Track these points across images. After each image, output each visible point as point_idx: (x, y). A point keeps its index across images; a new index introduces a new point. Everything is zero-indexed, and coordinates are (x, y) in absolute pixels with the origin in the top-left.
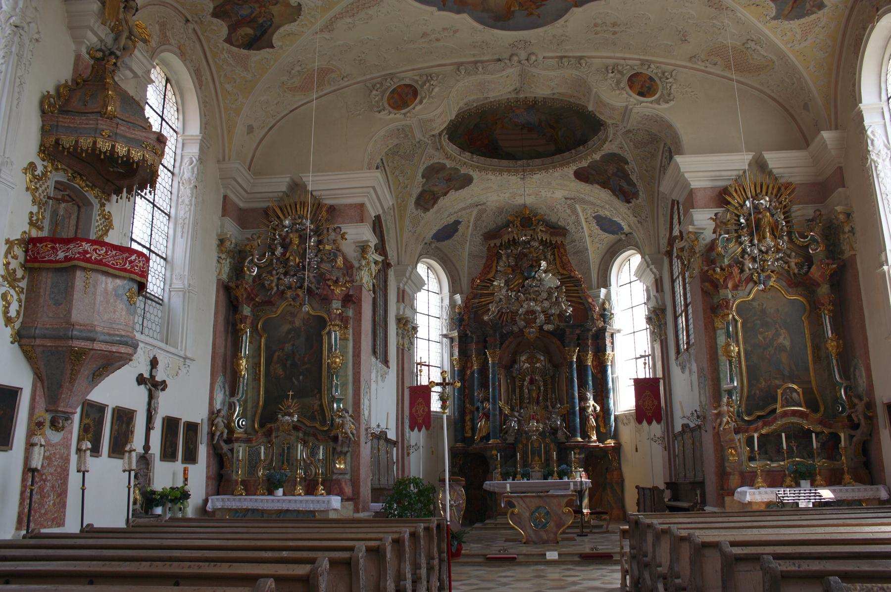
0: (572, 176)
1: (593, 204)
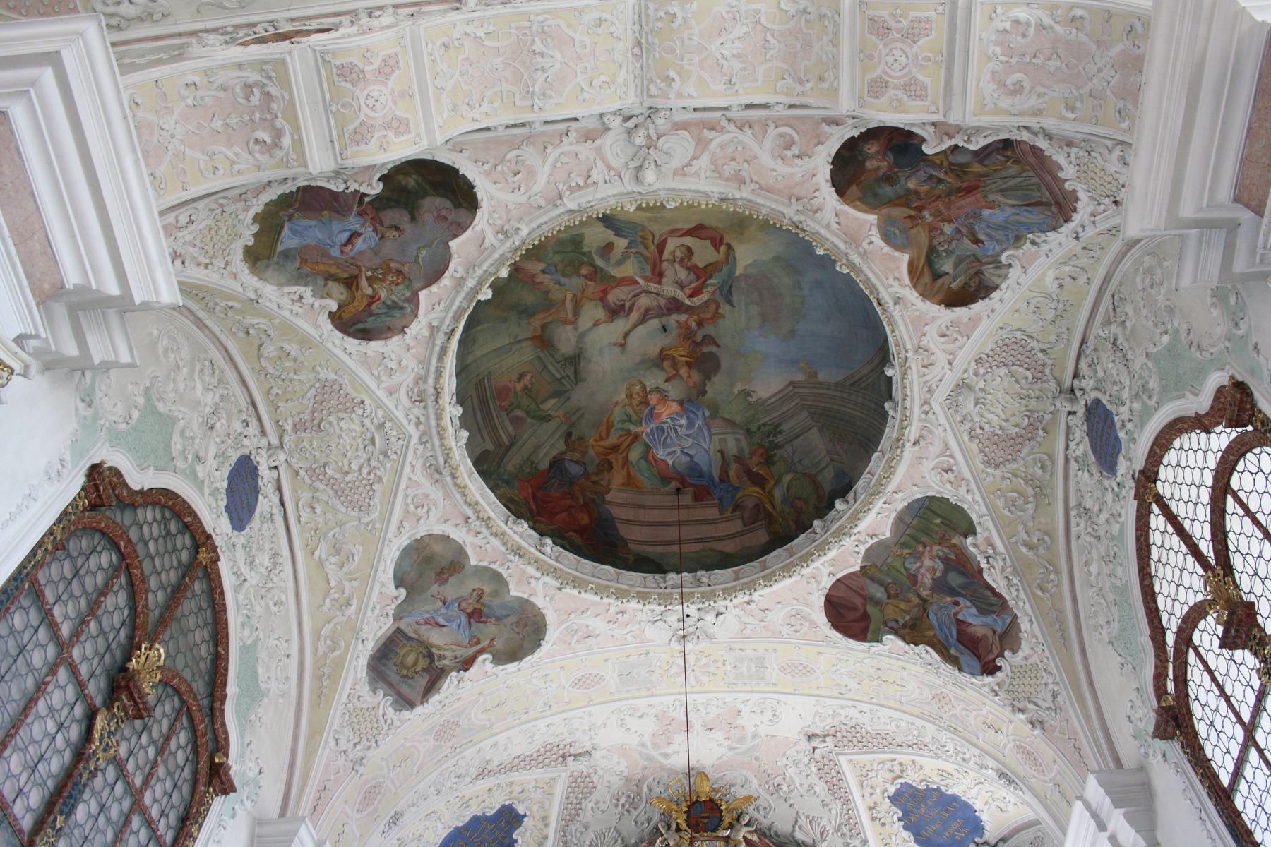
0: (821, 618)
1: (886, 742)
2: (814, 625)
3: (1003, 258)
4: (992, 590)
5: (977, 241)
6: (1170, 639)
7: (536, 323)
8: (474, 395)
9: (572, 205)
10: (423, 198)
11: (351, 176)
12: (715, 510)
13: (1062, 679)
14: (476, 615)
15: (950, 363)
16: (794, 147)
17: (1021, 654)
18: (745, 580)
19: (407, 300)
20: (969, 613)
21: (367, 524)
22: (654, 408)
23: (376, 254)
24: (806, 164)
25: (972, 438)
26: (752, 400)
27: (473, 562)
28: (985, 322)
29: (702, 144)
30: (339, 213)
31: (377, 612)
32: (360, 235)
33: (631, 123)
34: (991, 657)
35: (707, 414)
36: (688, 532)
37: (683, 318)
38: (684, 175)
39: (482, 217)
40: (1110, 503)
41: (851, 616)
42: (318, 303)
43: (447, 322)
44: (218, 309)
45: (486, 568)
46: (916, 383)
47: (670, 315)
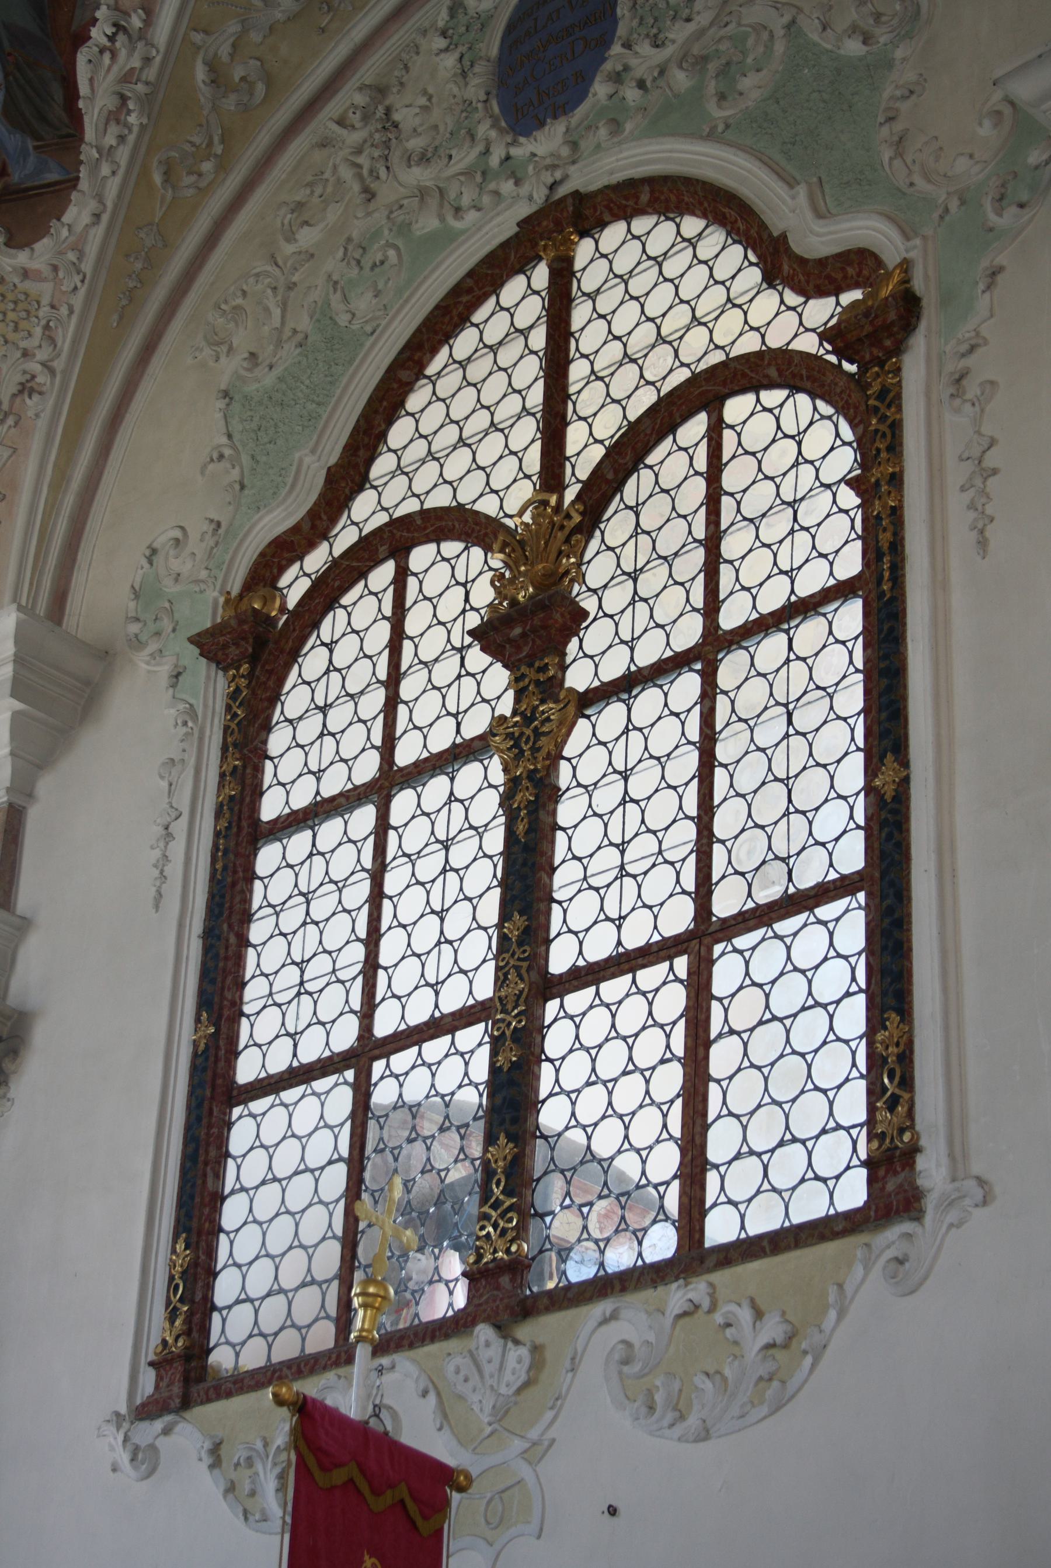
4: (72, 93)
6: (366, 512)
13: (66, 373)
17: (22, 258)
40: (457, 167)
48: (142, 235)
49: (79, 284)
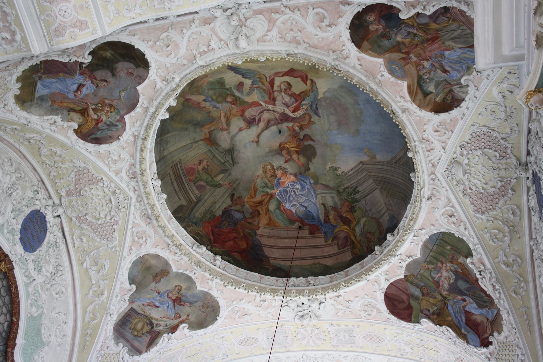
0: (383, 307)
2: (379, 311)
3: (462, 81)
4: (485, 292)
5: (445, 71)
7: (206, 130)
8: (171, 173)
9: (201, 63)
10: (117, 63)
11: (72, 53)
12: (322, 240)
14: (178, 301)
15: (444, 148)
16: (325, 20)
18: (335, 283)
19: (118, 121)
20: (472, 307)
21: (112, 248)
22: (280, 179)
23: (95, 96)
24: (334, 30)
25: (465, 195)
26: (339, 172)
27: (174, 270)
28: (461, 122)
29: (272, 22)
30: (69, 74)
31: (119, 298)
32: (84, 85)
33: (229, 13)
34: (486, 335)
35: (312, 181)
36: (298, 253)
37: (290, 125)
38: (264, 41)
39: (153, 73)
41: (401, 306)
42: (66, 124)
43: (142, 133)
44: (8, 130)
45: (182, 274)
46: (423, 161)
47: (282, 123)
48: (521, 310)
49: (134, 220)
